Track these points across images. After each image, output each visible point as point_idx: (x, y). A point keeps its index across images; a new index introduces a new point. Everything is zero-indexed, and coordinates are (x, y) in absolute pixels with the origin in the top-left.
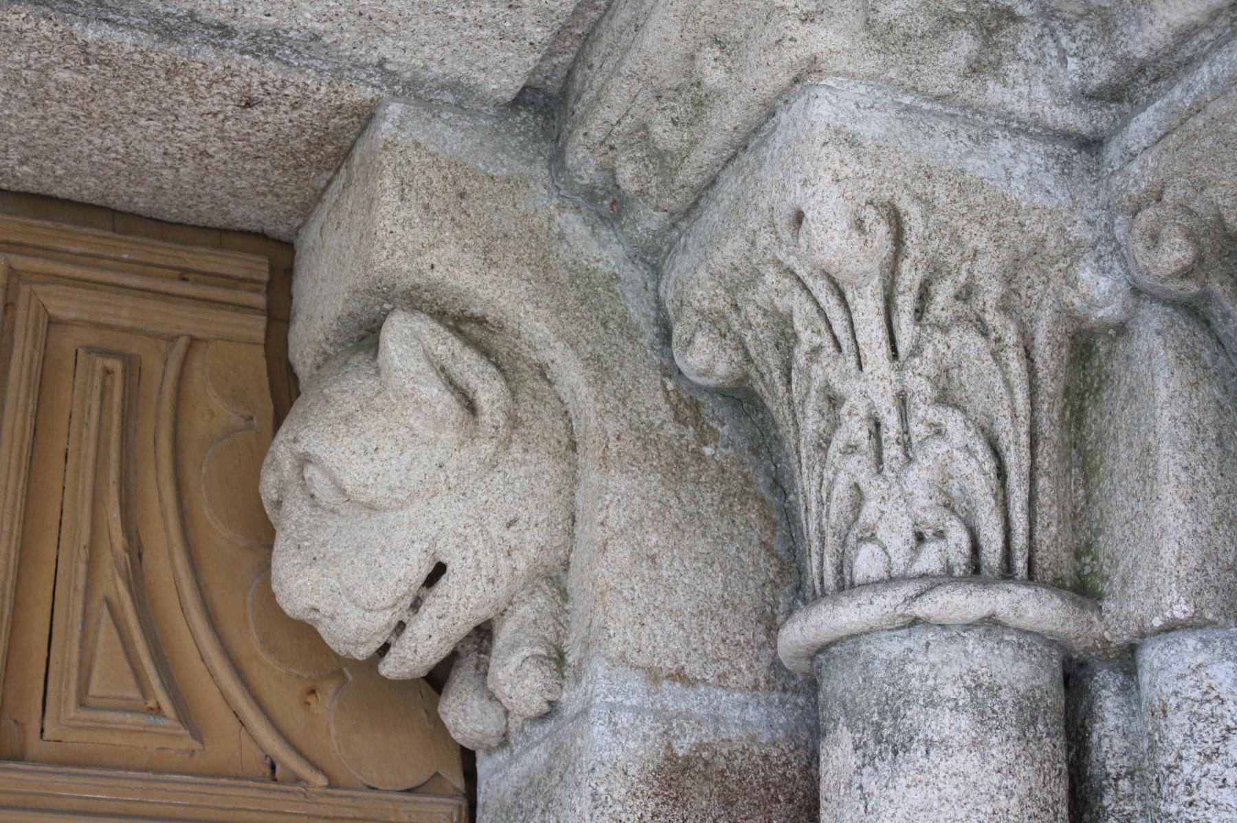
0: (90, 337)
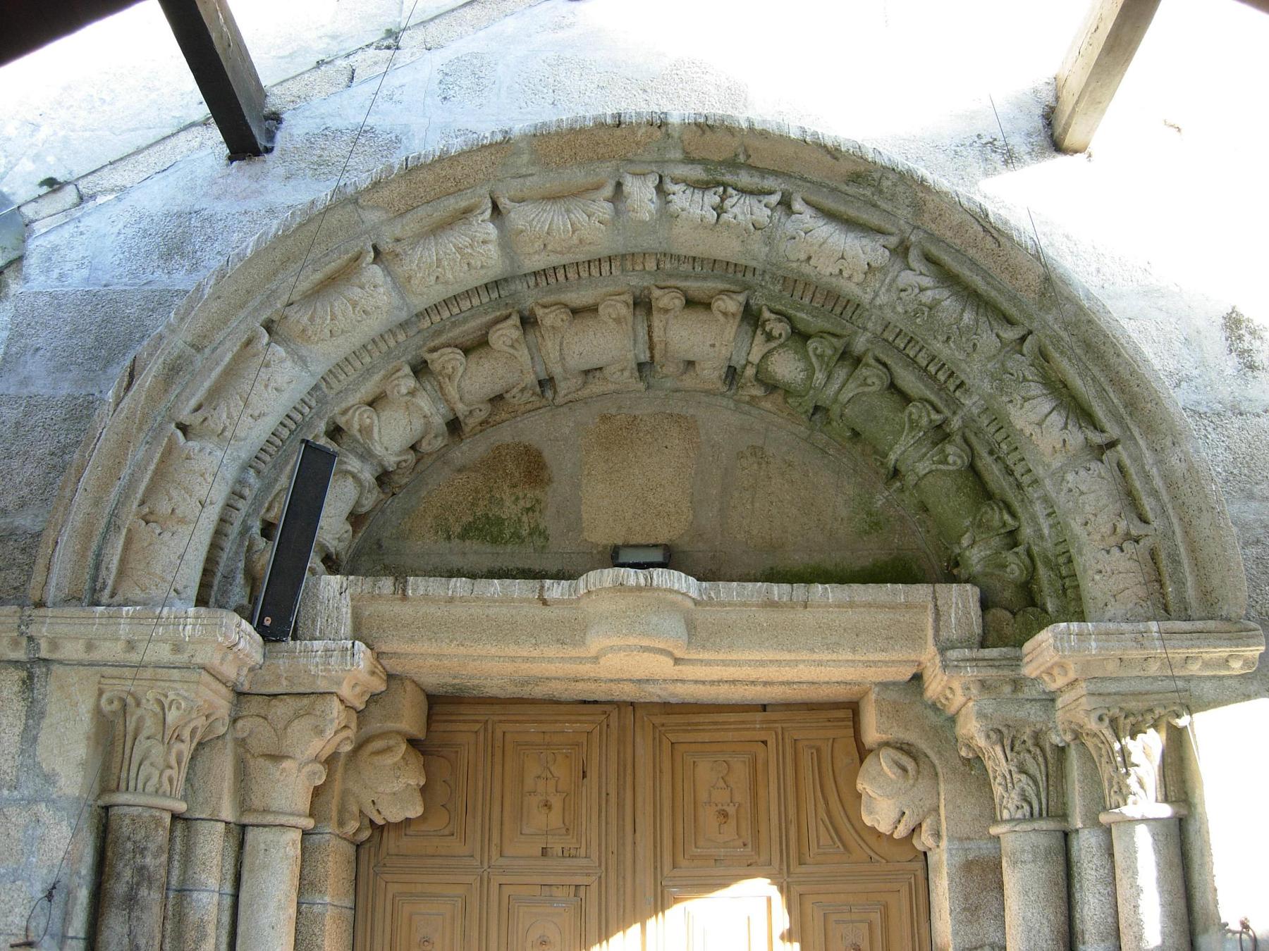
0: (806, 743)
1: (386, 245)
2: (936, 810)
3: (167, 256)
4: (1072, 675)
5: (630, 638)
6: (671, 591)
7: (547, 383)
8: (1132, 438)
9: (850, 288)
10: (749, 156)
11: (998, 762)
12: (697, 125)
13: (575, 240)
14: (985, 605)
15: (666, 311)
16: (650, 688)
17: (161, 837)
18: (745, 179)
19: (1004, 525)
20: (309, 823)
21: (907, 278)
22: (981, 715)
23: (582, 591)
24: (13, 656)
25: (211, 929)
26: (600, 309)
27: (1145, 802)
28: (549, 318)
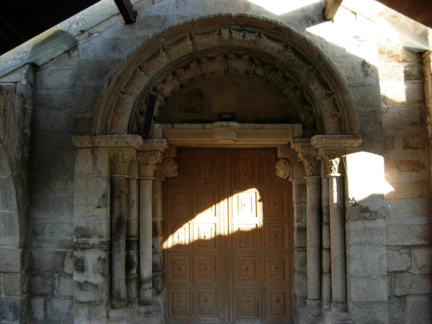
1: (166, 46)
2: (293, 173)
3: (113, 50)
4: (320, 146)
5: (225, 136)
6: (233, 126)
7: (203, 75)
8: (337, 92)
9: (274, 55)
10: (251, 23)
11: (306, 163)
12: (238, 16)
13: (210, 44)
14: (304, 128)
15: (231, 59)
16: (229, 146)
17: (124, 183)
18: (250, 29)
19: (309, 109)
20: (154, 178)
21: (287, 53)
22: (302, 153)
23: (214, 127)
24: (89, 146)
25: (135, 202)
26: (216, 58)
27: (335, 173)
28: (204, 61)
